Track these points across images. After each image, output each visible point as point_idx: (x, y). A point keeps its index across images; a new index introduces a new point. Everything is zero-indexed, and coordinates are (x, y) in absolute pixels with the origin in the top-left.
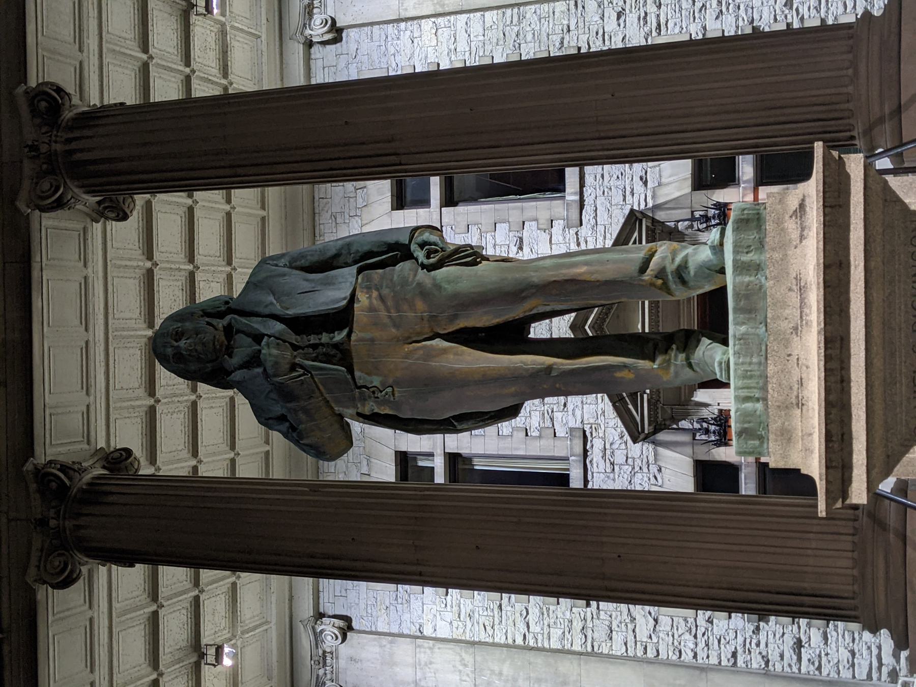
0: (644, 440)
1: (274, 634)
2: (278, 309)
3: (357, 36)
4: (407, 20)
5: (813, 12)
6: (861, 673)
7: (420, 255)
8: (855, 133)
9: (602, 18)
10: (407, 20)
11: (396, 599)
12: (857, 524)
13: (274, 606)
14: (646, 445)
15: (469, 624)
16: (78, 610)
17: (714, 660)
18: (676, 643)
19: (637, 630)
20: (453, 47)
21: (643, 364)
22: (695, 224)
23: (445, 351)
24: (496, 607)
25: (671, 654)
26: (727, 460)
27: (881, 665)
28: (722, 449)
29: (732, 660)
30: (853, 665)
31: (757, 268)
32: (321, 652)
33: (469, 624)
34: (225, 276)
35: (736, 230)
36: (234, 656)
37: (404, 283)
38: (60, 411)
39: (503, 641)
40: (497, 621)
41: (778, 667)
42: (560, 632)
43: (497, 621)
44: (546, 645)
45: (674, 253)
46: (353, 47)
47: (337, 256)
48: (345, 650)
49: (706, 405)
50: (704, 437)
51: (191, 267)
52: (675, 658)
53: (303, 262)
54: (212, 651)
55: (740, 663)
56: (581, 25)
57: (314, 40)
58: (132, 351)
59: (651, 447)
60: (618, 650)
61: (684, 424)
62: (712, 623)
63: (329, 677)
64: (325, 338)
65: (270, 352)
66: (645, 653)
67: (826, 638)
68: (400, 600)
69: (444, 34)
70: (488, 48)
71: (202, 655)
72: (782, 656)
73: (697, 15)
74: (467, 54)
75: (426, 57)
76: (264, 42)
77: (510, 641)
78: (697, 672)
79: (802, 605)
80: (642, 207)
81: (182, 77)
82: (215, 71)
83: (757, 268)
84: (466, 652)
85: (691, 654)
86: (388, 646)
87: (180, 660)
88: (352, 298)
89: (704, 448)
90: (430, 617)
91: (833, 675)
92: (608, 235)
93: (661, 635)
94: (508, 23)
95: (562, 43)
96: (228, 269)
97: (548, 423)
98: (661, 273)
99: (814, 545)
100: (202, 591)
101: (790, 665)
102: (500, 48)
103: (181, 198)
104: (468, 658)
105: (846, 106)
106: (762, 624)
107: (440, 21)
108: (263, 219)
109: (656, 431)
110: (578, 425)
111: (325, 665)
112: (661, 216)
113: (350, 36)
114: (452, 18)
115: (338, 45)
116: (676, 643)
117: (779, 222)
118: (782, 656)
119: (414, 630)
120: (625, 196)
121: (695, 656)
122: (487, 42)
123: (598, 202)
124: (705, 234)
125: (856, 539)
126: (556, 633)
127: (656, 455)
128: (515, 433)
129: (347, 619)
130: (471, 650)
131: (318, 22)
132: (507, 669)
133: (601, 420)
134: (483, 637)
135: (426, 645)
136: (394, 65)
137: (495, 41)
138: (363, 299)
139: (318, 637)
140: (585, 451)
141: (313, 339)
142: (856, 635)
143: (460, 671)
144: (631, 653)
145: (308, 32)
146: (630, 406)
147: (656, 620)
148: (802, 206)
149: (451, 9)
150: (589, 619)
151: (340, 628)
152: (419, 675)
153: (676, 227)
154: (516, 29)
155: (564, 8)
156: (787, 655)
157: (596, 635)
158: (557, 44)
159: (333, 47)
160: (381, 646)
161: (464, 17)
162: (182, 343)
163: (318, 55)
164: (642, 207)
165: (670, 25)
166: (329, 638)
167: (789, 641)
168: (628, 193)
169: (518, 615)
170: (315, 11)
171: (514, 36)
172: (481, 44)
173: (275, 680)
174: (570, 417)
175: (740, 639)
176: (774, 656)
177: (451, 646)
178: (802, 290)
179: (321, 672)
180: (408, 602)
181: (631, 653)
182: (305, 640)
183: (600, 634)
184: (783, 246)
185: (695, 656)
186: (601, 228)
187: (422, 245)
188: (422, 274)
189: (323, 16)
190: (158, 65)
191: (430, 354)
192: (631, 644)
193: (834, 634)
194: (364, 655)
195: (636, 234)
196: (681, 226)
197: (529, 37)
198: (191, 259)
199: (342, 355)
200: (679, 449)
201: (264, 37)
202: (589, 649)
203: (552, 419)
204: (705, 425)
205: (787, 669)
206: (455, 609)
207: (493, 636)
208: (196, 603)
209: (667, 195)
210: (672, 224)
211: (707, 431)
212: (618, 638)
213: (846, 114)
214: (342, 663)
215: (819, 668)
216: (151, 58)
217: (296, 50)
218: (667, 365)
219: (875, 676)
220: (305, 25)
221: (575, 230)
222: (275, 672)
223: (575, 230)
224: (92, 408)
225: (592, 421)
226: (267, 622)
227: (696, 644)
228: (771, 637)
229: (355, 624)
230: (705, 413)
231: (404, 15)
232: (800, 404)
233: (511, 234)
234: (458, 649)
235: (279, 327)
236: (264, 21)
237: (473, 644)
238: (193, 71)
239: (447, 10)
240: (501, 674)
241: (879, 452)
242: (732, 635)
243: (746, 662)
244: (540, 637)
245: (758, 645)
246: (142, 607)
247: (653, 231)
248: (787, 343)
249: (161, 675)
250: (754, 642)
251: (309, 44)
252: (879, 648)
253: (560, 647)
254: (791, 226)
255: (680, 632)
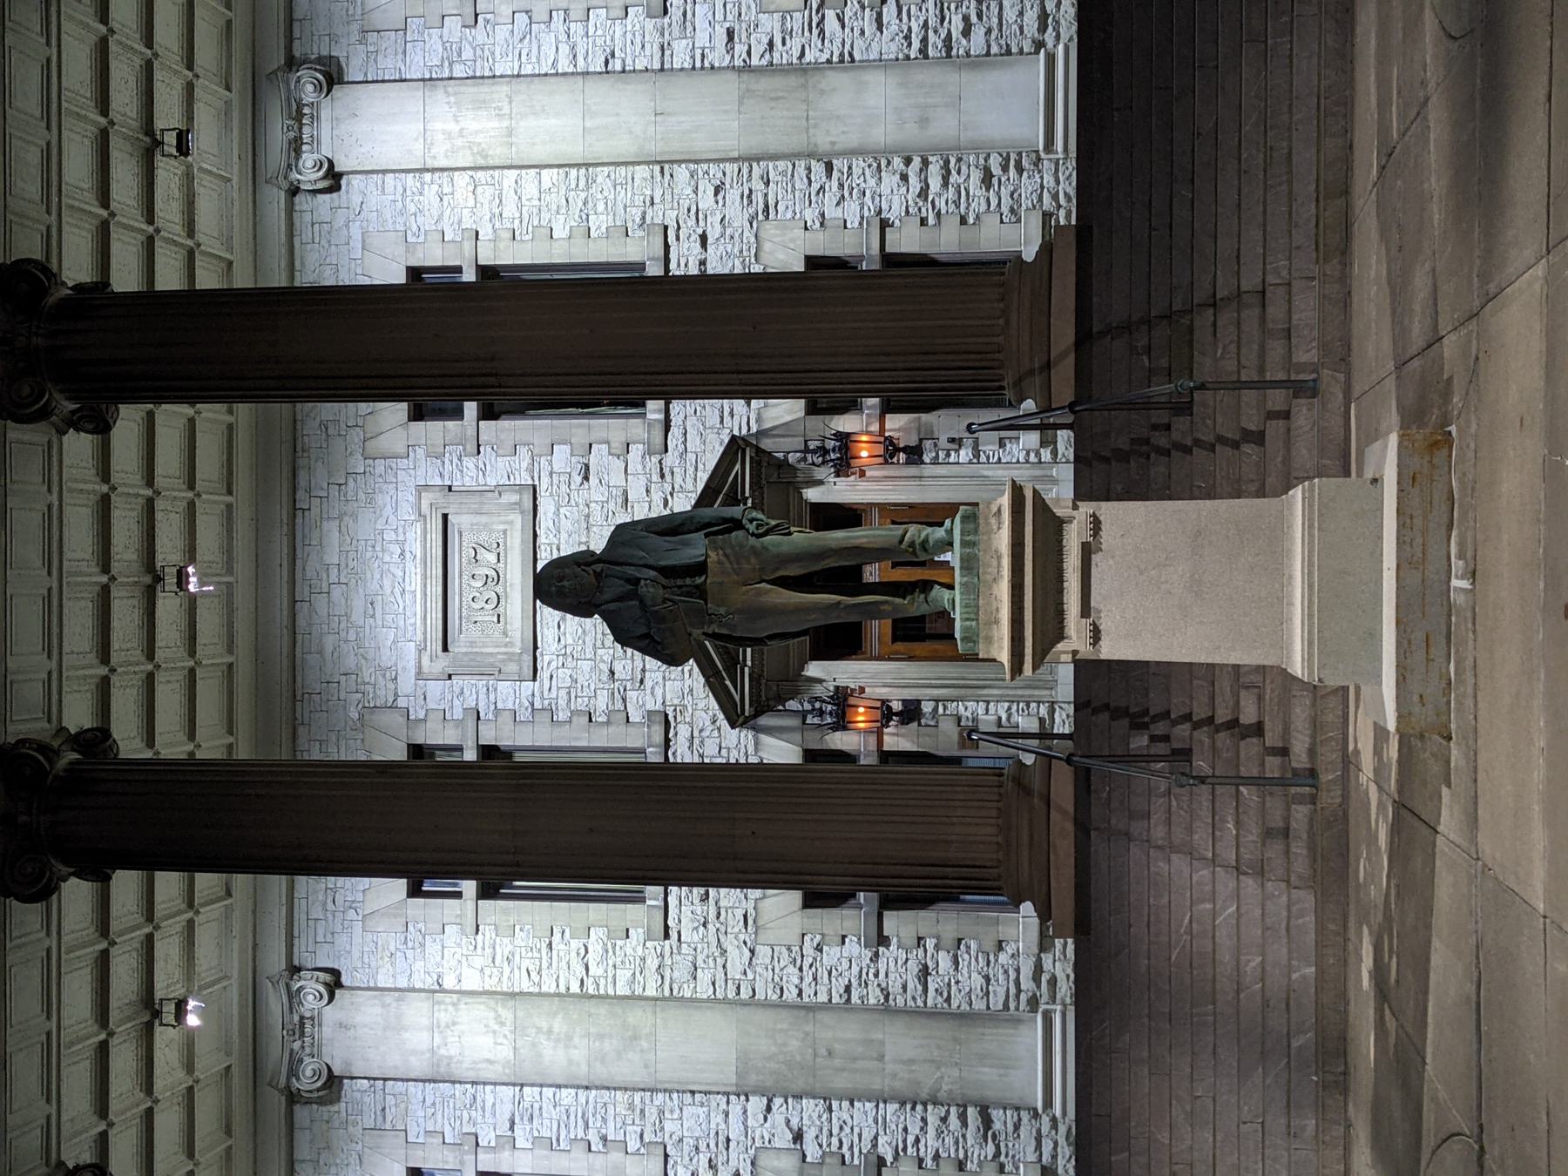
0: (741, 725)
1: (234, 994)
2: (651, 562)
3: (362, 185)
4: (434, 170)
5: (952, 208)
6: (997, 1002)
7: (752, 527)
8: (1004, 383)
9: (696, 191)
10: (434, 170)
11: (405, 943)
12: (1002, 790)
13: (235, 955)
14: (744, 732)
15: (507, 970)
16: (33, 937)
17: (823, 998)
18: (777, 979)
19: (728, 965)
20: (497, 212)
21: (898, 600)
22: (809, 456)
23: (767, 592)
24: (544, 946)
25: (770, 992)
26: (844, 748)
27: (1019, 991)
28: (838, 734)
29: (845, 996)
30: (988, 993)
31: (974, 544)
32: (296, 1018)
33: (507, 970)
34: (185, 504)
35: (962, 522)
36: (202, 1013)
37: (741, 546)
38: (21, 677)
39: (553, 990)
40: (545, 964)
41: (900, 1001)
42: (629, 974)
43: (545, 964)
44: (611, 992)
45: (920, 532)
46: (356, 199)
47: (682, 524)
48: (330, 1014)
49: (820, 681)
50: (816, 720)
51: (149, 492)
52: (775, 997)
53: (656, 529)
54: (170, 1008)
55: (855, 999)
56: (668, 197)
57: (303, 187)
58: (83, 603)
59: (750, 734)
60: (704, 991)
61: (793, 705)
62: (821, 951)
63: (308, 1050)
64: (688, 581)
65: (646, 589)
66: (738, 993)
67: (956, 963)
68: (410, 944)
69: (486, 193)
70: (545, 216)
71: (157, 1014)
72: (904, 987)
73: (813, 198)
74: (517, 222)
75: (460, 222)
76: (236, 187)
77: (562, 989)
78: (803, 1013)
79: (946, 878)
80: (744, 432)
81: (143, 238)
82: (178, 229)
83: (974, 544)
84: (504, 1007)
85: (795, 992)
86: (394, 1004)
87: (129, 1019)
88: (707, 556)
89: (817, 735)
90: (453, 963)
91: (965, 1007)
92: (700, 466)
93: (758, 969)
94: (573, 186)
95: (643, 218)
96: (190, 495)
97: (619, 705)
98: (912, 544)
99: (961, 797)
100: (157, 928)
101: (914, 998)
102: (562, 218)
103: (186, 410)
104: (507, 1015)
105: (996, 356)
106: (881, 949)
107: (480, 174)
108: (230, 427)
109: (757, 714)
110: (659, 707)
111: (302, 1034)
112: (767, 444)
113: (352, 185)
114: (496, 173)
115: (335, 195)
116: (777, 979)
117: (986, 519)
118: (904, 987)
119: (430, 982)
120: (722, 418)
121: (800, 994)
122: (544, 209)
123: (688, 424)
124: (822, 469)
125: (1000, 805)
126: (624, 975)
127: (757, 744)
128: (575, 719)
129: (336, 973)
130: (511, 1003)
131: (309, 164)
132: (558, 1025)
133: (688, 701)
134: (526, 986)
135: (448, 1000)
136: (415, 228)
137: (554, 207)
138: (712, 554)
139: (294, 997)
140: (667, 740)
141: (679, 582)
142: (992, 957)
143: (494, 1032)
144: (719, 996)
145: (294, 176)
146: (728, 682)
147: (752, 952)
148: (999, 510)
149: (497, 162)
150: (667, 954)
151: (326, 984)
152: (437, 1040)
153: (786, 458)
154: (583, 195)
155: (647, 175)
156: (910, 986)
157: (676, 974)
158: (638, 220)
159: (327, 197)
160: (384, 1006)
161: (513, 173)
162: (565, 583)
163: (305, 207)
164: (744, 432)
165: (781, 208)
166: (311, 997)
167: (913, 967)
168: (726, 414)
169: (573, 954)
170: (305, 148)
171: (580, 204)
172: (535, 211)
173: (235, 1054)
174: (649, 697)
175: (855, 970)
176: (894, 988)
177: (483, 999)
178: (999, 558)
179: (297, 1045)
180: (422, 945)
181: (719, 996)
182: (275, 1003)
183: (681, 973)
184: (989, 532)
185: (800, 994)
186: (691, 457)
187: (751, 521)
188: (752, 540)
189: (316, 156)
190: (204, 253)
191: (760, 593)
192: (720, 983)
193: (966, 957)
194: (358, 1019)
195: (738, 466)
196: (792, 458)
197: (601, 207)
198: (150, 482)
199: (701, 592)
200: (784, 736)
201: (235, 179)
202: (667, 993)
203: (624, 700)
204: (817, 705)
205: (911, 1003)
206: (488, 951)
207: (539, 985)
208: (149, 940)
209: (776, 418)
210: (780, 455)
211: (821, 713)
212: (704, 977)
213: (996, 364)
214: (327, 1031)
215: (948, 1000)
216: (113, 215)
217: (275, 199)
218: (912, 603)
219: (1012, 1005)
220: (289, 166)
221: (658, 457)
222: (236, 1047)
223: (658, 457)
224: (55, 676)
225: (676, 702)
226: (226, 977)
227: (802, 979)
228: (892, 964)
229: (345, 980)
230: (818, 690)
231: (430, 164)
232: (997, 622)
233: (574, 459)
234: (492, 1003)
235: (653, 573)
236: (236, 159)
237: (513, 995)
238: (158, 231)
239: (491, 163)
240: (550, 1031)
241: (1039, 651)
242: (845, 964)
243: (861, 998)
244: (602, 982)
245: (876, 975)
246: (179, 913)
247: (759, 463)
248: (990, 588)
249: (111, 1034)
250: (872, 971)
251: (294, 191)
252: (1018, 971)
253: (628, 993)
254: (993, 521)
255: (782, 964)
